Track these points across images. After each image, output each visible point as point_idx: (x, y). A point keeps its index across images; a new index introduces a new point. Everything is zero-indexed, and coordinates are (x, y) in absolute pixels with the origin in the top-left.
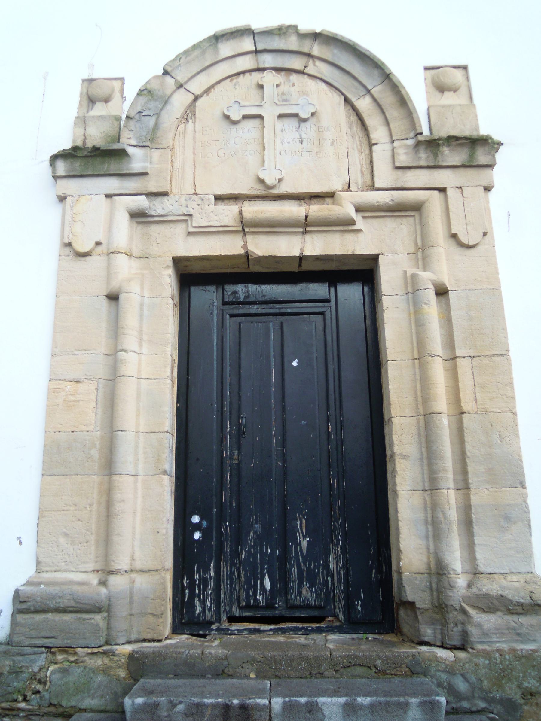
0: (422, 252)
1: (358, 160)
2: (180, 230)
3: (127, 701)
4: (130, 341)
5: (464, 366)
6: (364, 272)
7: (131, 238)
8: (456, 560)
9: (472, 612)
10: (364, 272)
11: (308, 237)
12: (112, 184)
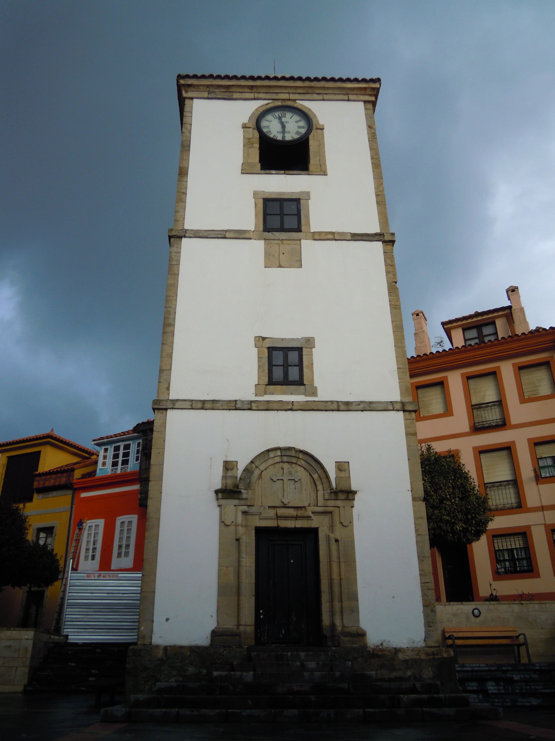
0: (332, 527)
1: (313, 495)
2: (257, 517)
3: (252, 654)
4: (243, 555)
5: (342, 565)
6: (315, 531)
7: (242, 520)
8: (338, 622)
9: (341, 637)
10: (315, 531)
11: (297, 521)
12: (236, 502)
